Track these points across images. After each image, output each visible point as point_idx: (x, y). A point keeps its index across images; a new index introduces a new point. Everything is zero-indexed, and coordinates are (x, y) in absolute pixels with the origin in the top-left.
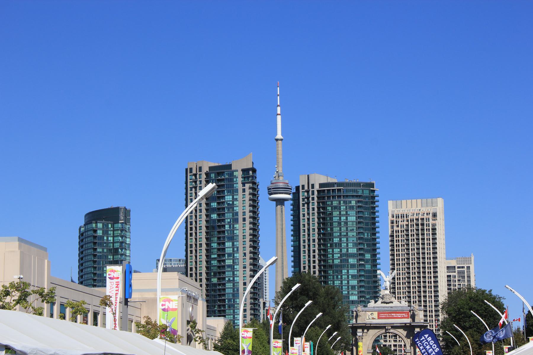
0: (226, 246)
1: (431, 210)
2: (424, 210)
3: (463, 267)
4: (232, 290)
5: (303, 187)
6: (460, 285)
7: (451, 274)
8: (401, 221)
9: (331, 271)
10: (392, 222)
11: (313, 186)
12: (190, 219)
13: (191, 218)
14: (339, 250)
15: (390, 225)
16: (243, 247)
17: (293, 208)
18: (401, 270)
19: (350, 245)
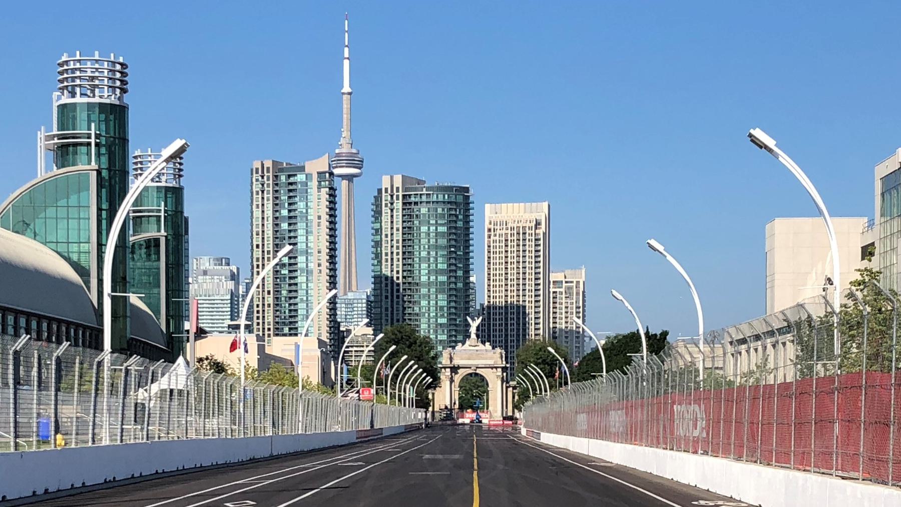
0: (300, 325)
1: (534, 216)
2: (527, 217)
3: (572, 282)
4: (305, 311)
5: (386, 190)
6: (567, 302)
7: (558, 290)
8: (500, 230)
9: (418, 222)
10: (489, 230)
11: (398, 189)
12: (256, 201)
13: (258, 266)
14: (427, 265)
15: (486, 233)
16: (318, 202)
17: (375, 281)
18: (498, 325)
19: (440, 260)
